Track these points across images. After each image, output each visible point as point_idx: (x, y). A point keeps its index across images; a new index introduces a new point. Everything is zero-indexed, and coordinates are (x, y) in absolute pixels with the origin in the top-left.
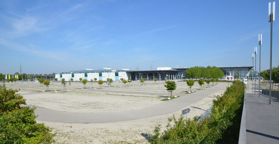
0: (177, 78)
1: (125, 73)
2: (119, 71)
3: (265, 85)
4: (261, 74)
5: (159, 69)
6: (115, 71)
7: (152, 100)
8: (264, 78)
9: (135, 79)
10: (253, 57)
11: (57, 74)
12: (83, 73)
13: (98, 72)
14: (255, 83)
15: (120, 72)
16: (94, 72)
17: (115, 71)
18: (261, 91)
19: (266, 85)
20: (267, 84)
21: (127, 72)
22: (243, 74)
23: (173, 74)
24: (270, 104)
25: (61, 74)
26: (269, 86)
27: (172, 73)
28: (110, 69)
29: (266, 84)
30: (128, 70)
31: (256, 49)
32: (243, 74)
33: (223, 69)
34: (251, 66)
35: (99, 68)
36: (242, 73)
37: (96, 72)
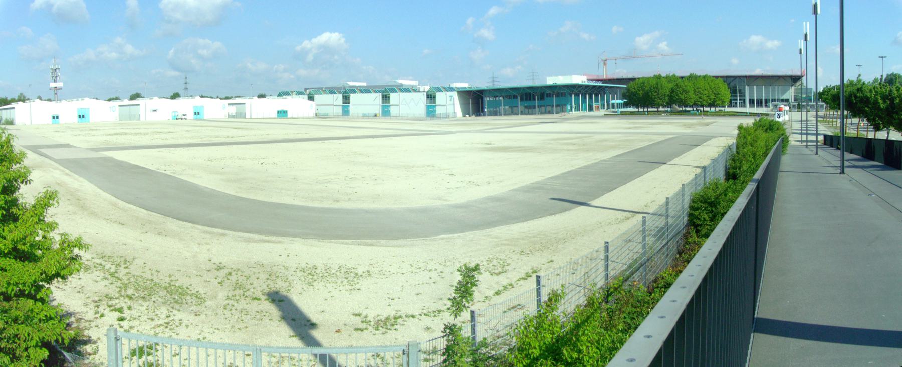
0: (603, 107)
1: (455, 95)
2: (439, 90)
3: (829, 122)
4: (821, 96)
5: (550, 81)
6: (427, 89)
7: (200, 303)
8: (826, 103)
9: (483, 111)
10: (801, 50)
11: (22, 99)
12: (340, 93)
13: (379, 92)
14: (806, 140)
15: (442, 91)
16: (368, 92)
17: (427, 90)
18: (821, 138)
19: (833, 122)
20: (835, 120)
21: (460, 92)
22: (778, 93)
23: (577, 95)
24: (843, 172)
25: (345, 92)
26: (839, 125)
27: (596, 92)
28: (414, 83)
29: (831, 120)
30: (465, 86)
31: (808, 28)
32: (778, 93)
33: (729, 80)
34: (798, 73)
35: (386, 81)
36: (777, 92)
37: (375, 92)
